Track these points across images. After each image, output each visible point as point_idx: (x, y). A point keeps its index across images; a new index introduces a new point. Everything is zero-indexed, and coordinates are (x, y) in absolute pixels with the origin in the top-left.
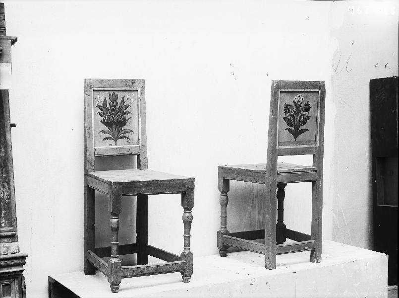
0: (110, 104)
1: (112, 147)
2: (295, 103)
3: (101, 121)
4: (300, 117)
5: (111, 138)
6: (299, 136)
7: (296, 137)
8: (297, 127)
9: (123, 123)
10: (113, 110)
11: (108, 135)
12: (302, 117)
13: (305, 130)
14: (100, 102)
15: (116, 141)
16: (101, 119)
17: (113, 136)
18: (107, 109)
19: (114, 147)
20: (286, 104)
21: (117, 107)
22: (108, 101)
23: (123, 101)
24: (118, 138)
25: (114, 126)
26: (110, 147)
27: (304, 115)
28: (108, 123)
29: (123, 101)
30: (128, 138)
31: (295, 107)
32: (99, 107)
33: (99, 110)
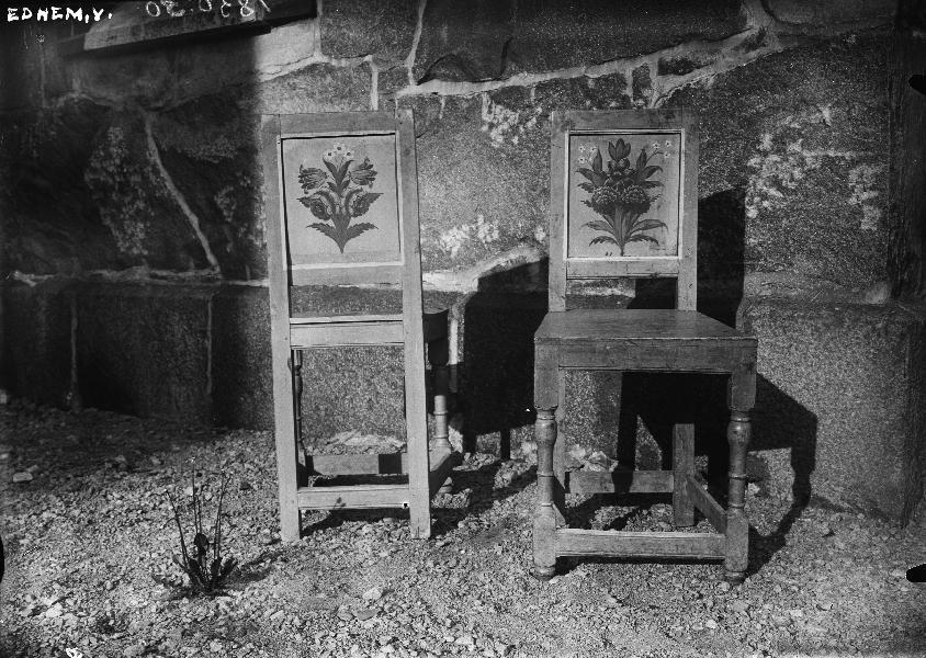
0: (610, 166)
1: (611, 259)
2: (328, 165)
3: (587, 202)
4: (349, 197)
5: (610, 239)
6: (350, 241)
7: (341, 246)
8: (342, 219)
9: (644, 206)
10: (616, 178)
11: (600, 233)
12: (355, 197)
13: (368, 226)
14: (586, 162)
15: (622, 248)
16: (587, 196)
17: (616, 234)
18: (604, 176)
19: (618, 258)
20: (305, 168)
21: (627, 172)
22: (606, 158)
23: (643, 158)
24: (627, 239)
25: (618, 213)
26: (607, 258)
27: (358, 191)
28: (606, 208)
29: (643, 158)
30: (652, 240)
31: (329, 174)
32: (584, 172)
33: (583, 180)
